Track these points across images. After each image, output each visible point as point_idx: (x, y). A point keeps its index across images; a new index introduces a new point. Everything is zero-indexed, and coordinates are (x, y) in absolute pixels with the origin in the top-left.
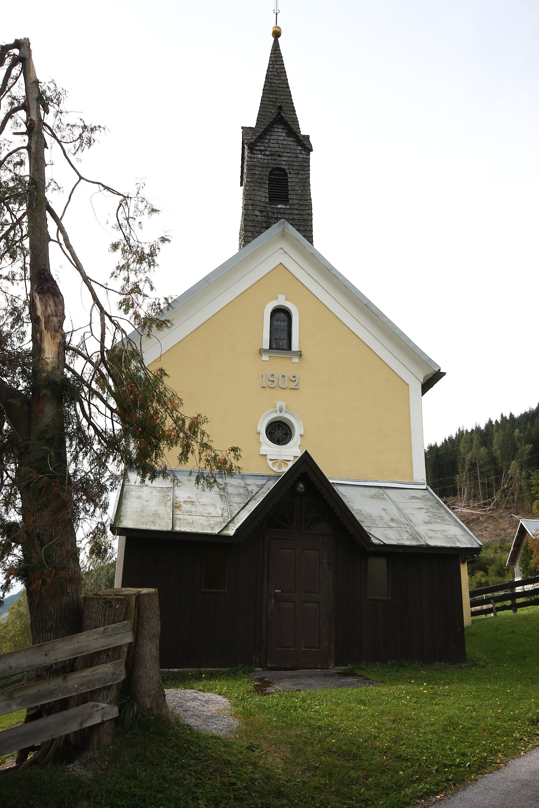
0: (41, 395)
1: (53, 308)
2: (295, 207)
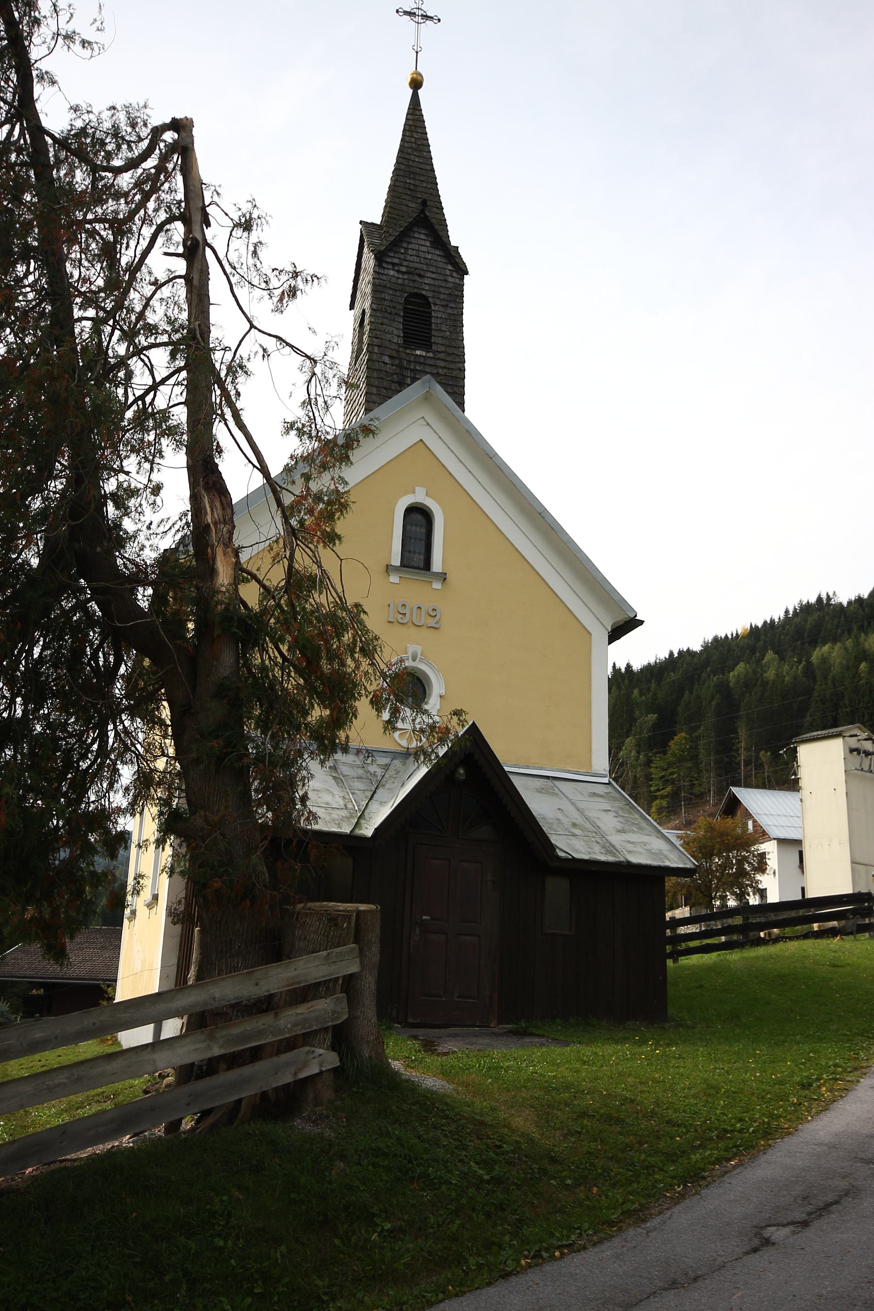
0: (215, 636)
1: (220, 512)
2: (441, 356)
